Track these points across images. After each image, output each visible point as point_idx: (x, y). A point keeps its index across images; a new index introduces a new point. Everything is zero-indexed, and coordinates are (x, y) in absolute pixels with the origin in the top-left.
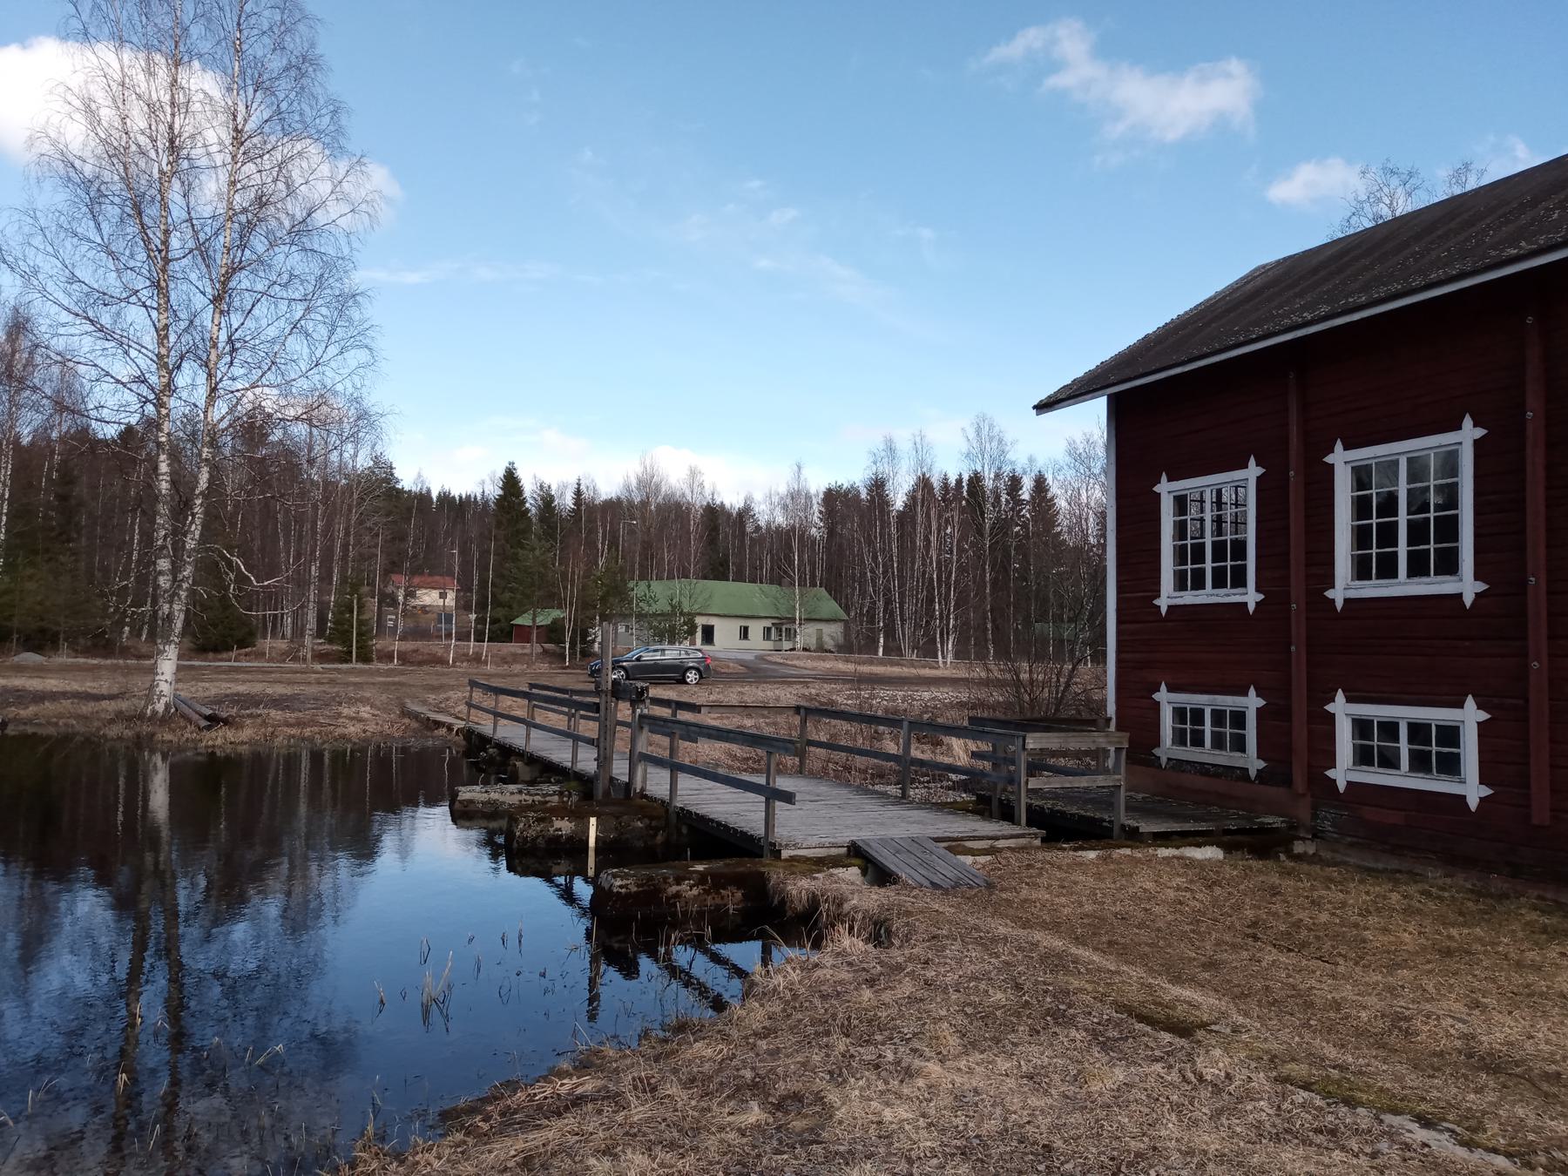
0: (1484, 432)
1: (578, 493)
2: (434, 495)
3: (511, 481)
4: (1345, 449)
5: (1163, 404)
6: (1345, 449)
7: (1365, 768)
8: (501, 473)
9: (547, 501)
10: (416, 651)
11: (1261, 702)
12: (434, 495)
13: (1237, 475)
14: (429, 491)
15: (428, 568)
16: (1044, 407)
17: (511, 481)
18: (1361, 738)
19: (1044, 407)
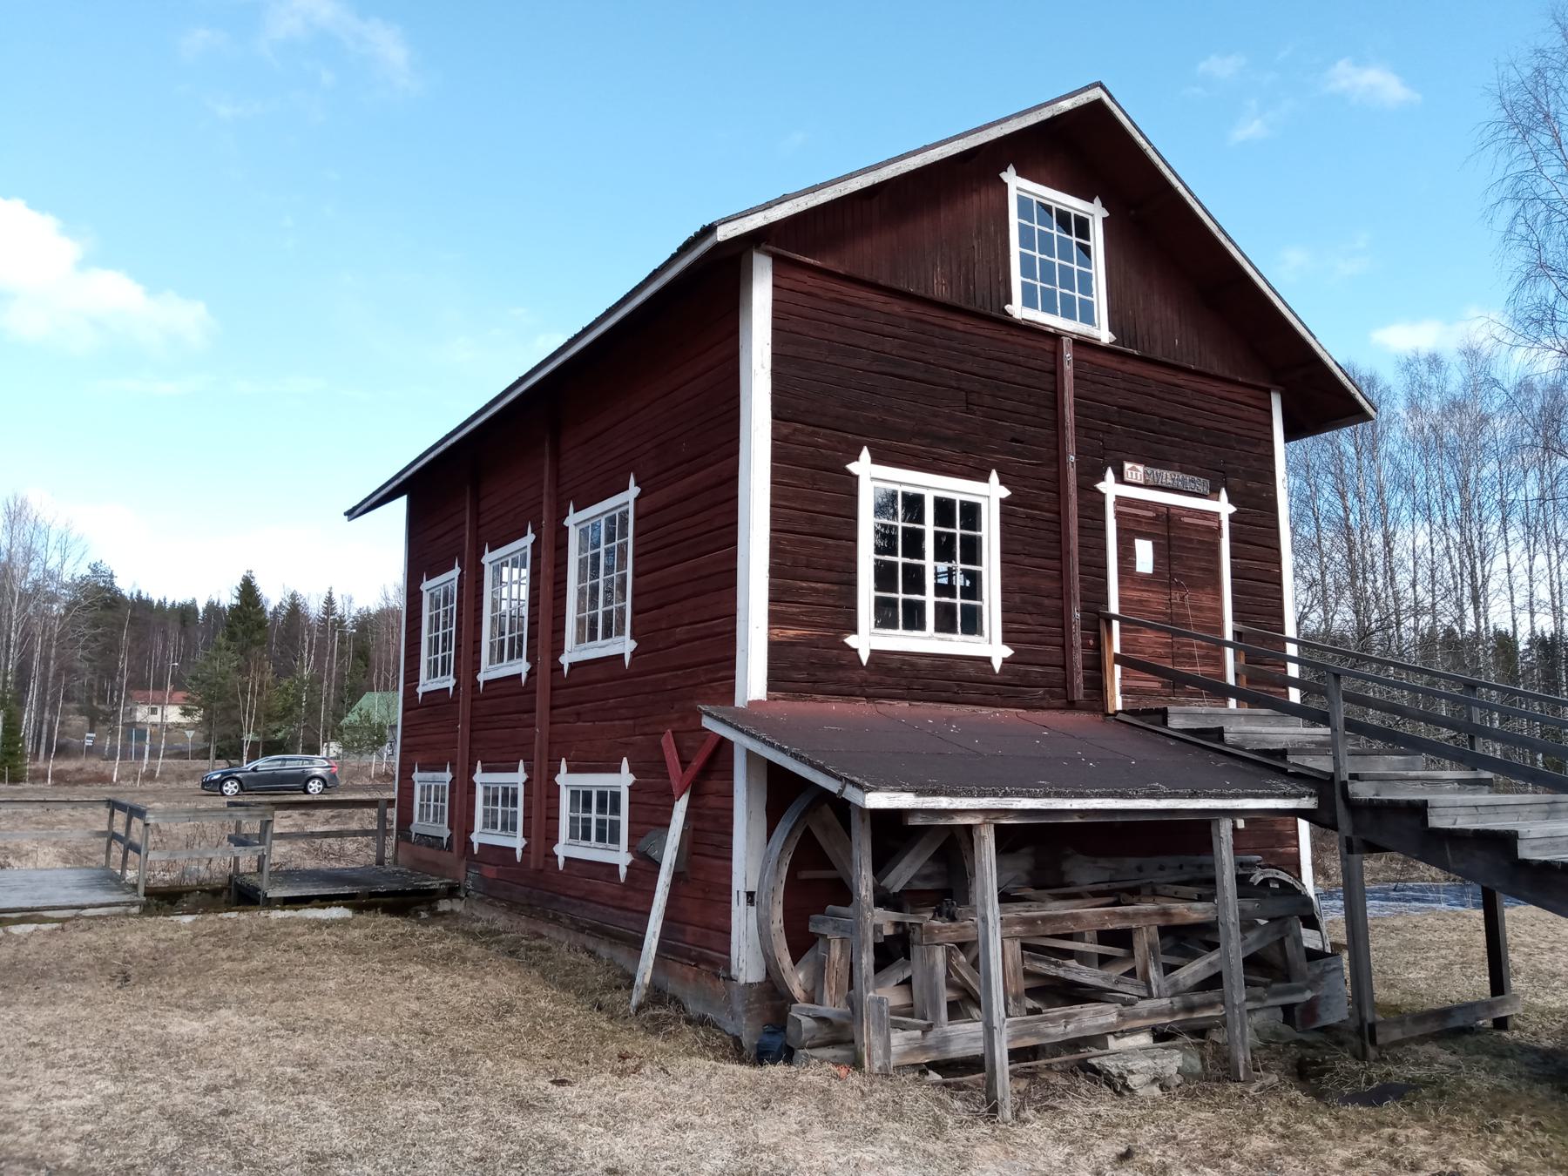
0: (865, 449)
1: (330, 601)
2: (201, 606)
3: (248, 590)
4: (855, 631)
5: (458, 494)
6: (855, 631)
7: (916, 633)
8: (238, 582)
9: (295, 610)
10: (80, 770)
11: (1005, 493)
12: (201, 606)
13: (438, 775)
14: (194, 601)
15: (146, 684)
16: (352, 514)
17: (248, 590)
18: (974, 537)
19: (352, 514)
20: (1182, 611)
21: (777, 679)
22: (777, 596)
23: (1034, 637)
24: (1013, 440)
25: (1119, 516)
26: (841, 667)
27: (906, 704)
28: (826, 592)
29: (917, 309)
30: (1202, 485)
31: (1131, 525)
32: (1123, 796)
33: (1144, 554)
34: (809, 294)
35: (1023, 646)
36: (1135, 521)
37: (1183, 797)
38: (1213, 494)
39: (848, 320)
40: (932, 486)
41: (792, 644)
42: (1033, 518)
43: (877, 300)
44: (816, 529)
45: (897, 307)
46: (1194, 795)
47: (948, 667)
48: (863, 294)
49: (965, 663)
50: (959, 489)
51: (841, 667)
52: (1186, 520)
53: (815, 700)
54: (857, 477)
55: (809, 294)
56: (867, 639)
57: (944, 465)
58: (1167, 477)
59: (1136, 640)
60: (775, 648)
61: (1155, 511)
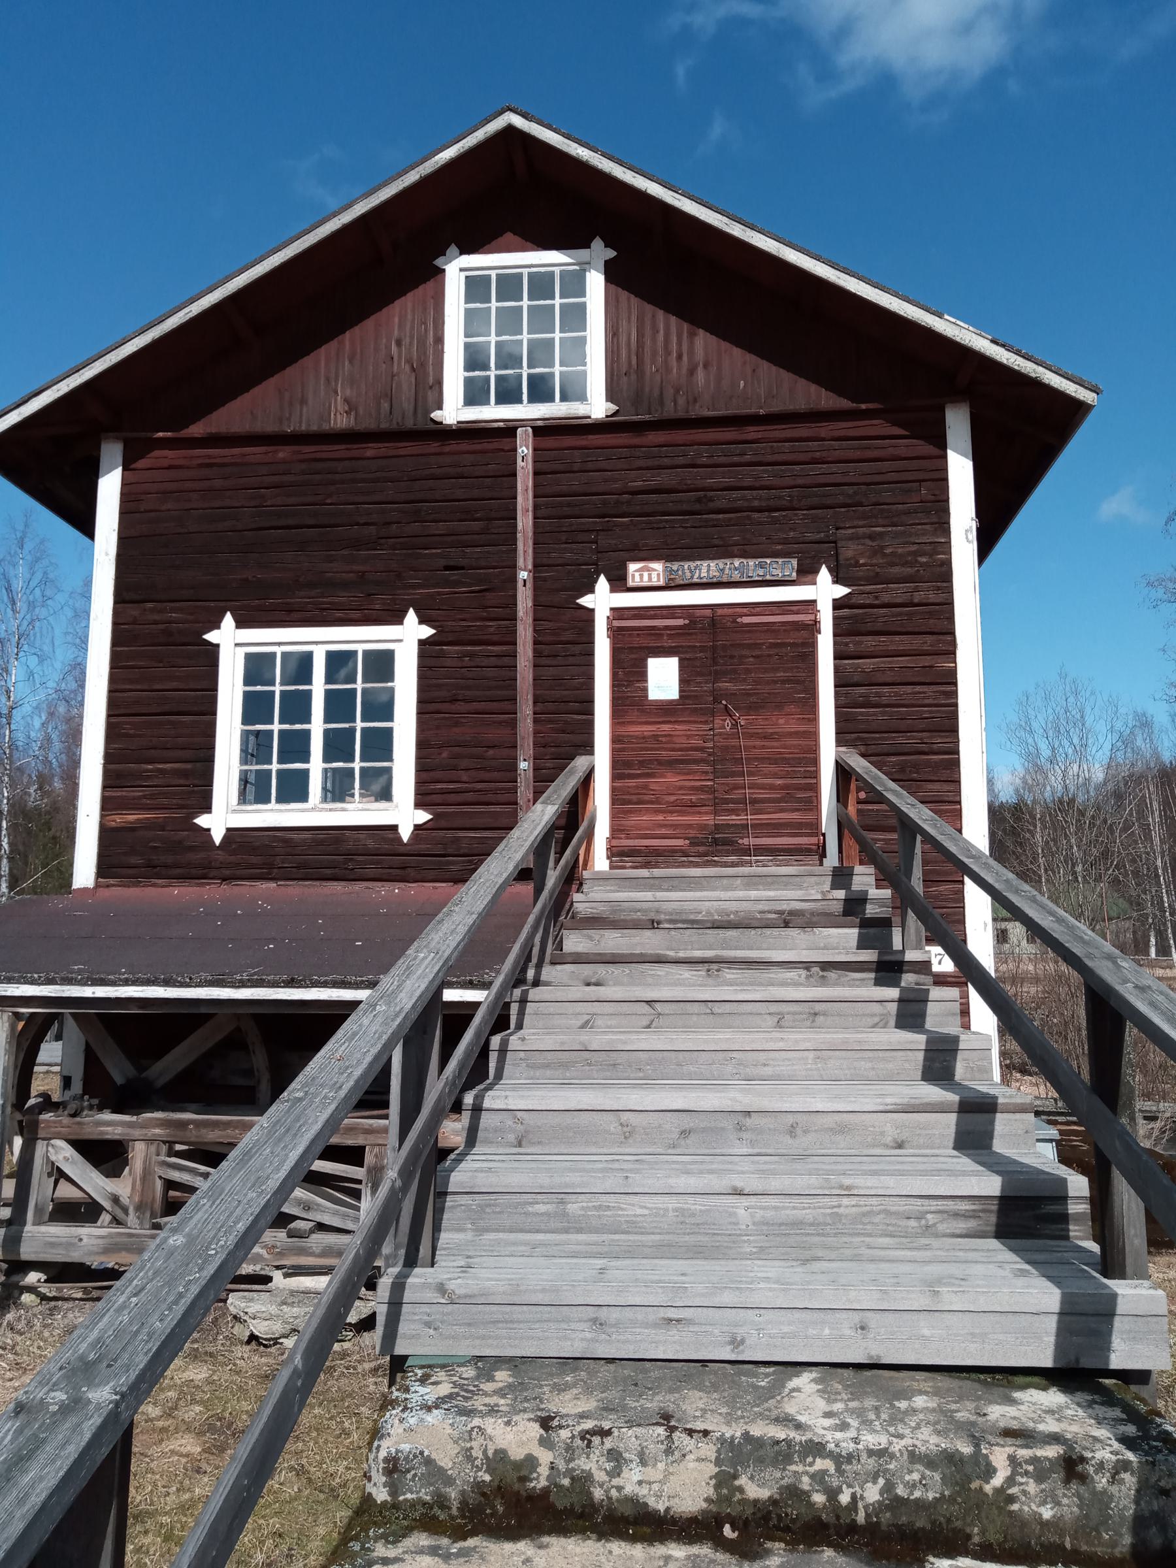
20: (734, 742)
21: (105, 867)
22: (111, 780)
23: (470, 797)
24: (447, 568)
25: (615, 633)
26: (191, 849)
27: (273, 885)
28: (176, 772)
29: (308, 450)
30: (789, 567)
31: (637, 642)
32: (167, 983)
33: (663, 678)
34: (170, 467)
35: (441, 809)
36: (637, 640)
37: (274, 985)
38: (806, 573)
39: (218, 483)
40: (319, 640)
41: (133, 829)
42: (471, 655)
43: (255, 453)
44: (166, 708)
45: (283, 453)
46: (291, 983)
47: (337, 841)
48: (236, 451)
49: (362, 835)
50: (360, 638)
51: (191, 849)
52: (746, 620)
53: (154, 885)
54: (400, 622)
55: (170, 467)
56: (222, 817)
57: (339, 614)
58: (707, 568)
59: (646, 787)
60: (106, 834)
61: (689, 617)
